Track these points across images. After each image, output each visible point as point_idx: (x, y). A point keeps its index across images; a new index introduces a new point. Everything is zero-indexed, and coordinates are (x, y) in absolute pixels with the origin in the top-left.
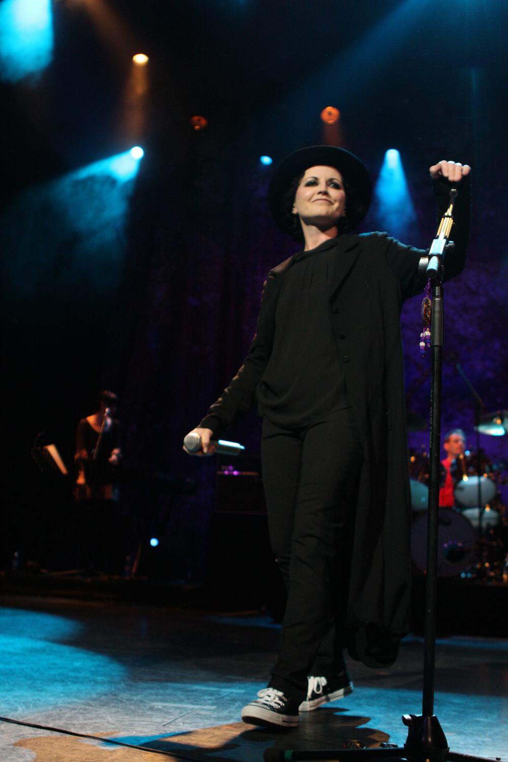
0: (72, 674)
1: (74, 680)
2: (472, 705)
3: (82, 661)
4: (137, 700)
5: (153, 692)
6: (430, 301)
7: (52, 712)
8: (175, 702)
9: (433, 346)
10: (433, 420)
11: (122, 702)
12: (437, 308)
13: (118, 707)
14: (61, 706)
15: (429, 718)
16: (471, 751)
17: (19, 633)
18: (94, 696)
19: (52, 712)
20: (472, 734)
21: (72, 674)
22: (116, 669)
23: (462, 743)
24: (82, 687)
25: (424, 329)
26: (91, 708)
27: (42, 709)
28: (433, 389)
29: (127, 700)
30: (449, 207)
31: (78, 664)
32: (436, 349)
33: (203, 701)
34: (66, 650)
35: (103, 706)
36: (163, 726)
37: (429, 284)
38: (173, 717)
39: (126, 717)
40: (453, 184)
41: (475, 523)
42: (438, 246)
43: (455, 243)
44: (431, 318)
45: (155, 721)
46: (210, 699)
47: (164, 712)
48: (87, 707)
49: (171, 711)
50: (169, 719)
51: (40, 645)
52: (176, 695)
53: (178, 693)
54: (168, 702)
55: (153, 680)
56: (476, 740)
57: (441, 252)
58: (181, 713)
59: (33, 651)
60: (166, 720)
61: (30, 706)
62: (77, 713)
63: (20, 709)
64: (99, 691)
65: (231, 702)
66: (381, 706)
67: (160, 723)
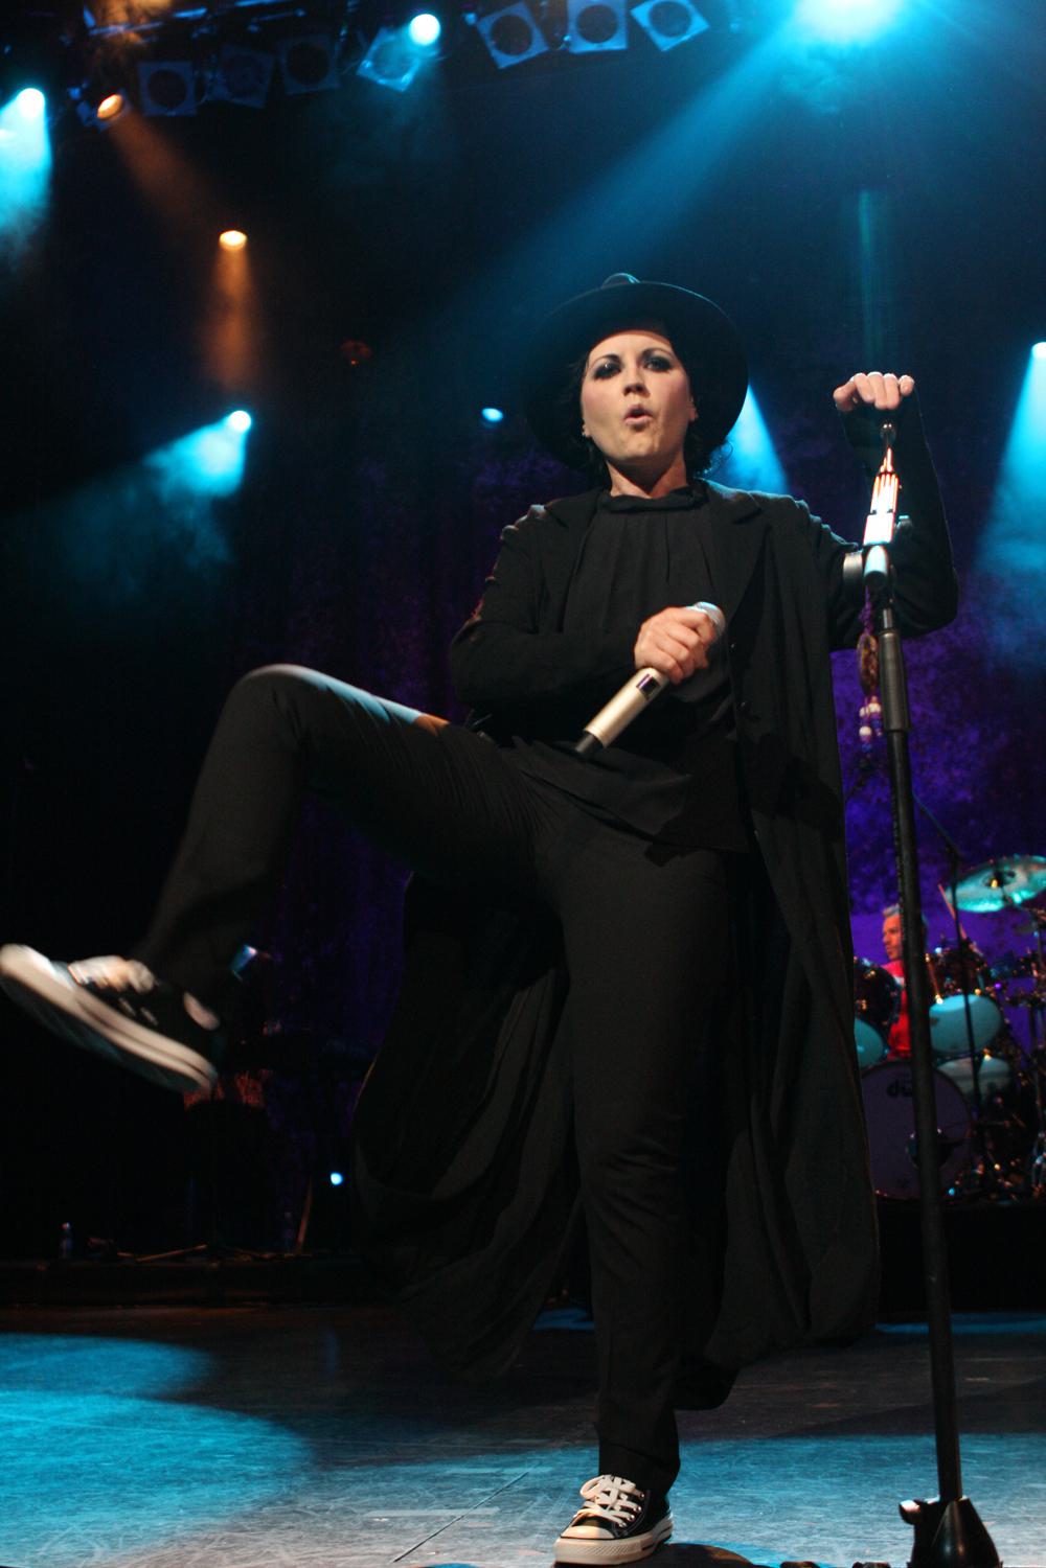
0: (199, 1464)
1: (204, 1476)
2: (1011, 1455)
3: (218, 1435)
4: (336, 1510)
5: (367, 1488)
6: (873, 641)
7: (166, 1552)
8: (414, 1507)
9: (888, 733)
10: (903, 884)
11: (307, 1516)
12: (890, 654)
13: (299, 1529)
14: (183, 1537)
15: (955, 1503)
16: (1034, 1558)
17: (84, 1386)
18: (248, 1508)
19: (166, 1552)
20: (1028, 1519)
21: (199, 1464)
22: (286, 1446)
23: (1011, 1541)
24: (222, 1492)
25: (866, 700)
26: (242, 1535)
27: (143, 1547)
28: (897, 820)
29: (316, 1511)
30: (885, 455)
31: (207, 1442)
32: (896, 738)
33: (470, 1499)
34: (182, 1414)
35: (267, 1528)
36: (396, 1561)
37: (867, 606)
38: (413, 1540)
39: (318, 1549)
40: (886, 414)
41: (966, 1086)
42: (880, 526)
43: (911, 518)
44: (878, 676)
45: (377, 1551)
46: (484, 1494)
47: (392, 1529)
48: (236, 1534)
49: (408, 1526)
50: (408, 1544)
51: (128, 1406)
52: (413, 1491)
53: (418, 1486)
54: (401, 1508)
55: (362, 1463)
56: (1039, 1533)
57: (888, 538)
58: (429, 1529)
59: (113, 1422)
60: (402, 1547)
61: (118, 1543)
62: (217, 1549)
63: (98, 1549)
64: (257, 1497)
65: (529, 1496)
66: (832, 1475)
67: (390, 1555)
